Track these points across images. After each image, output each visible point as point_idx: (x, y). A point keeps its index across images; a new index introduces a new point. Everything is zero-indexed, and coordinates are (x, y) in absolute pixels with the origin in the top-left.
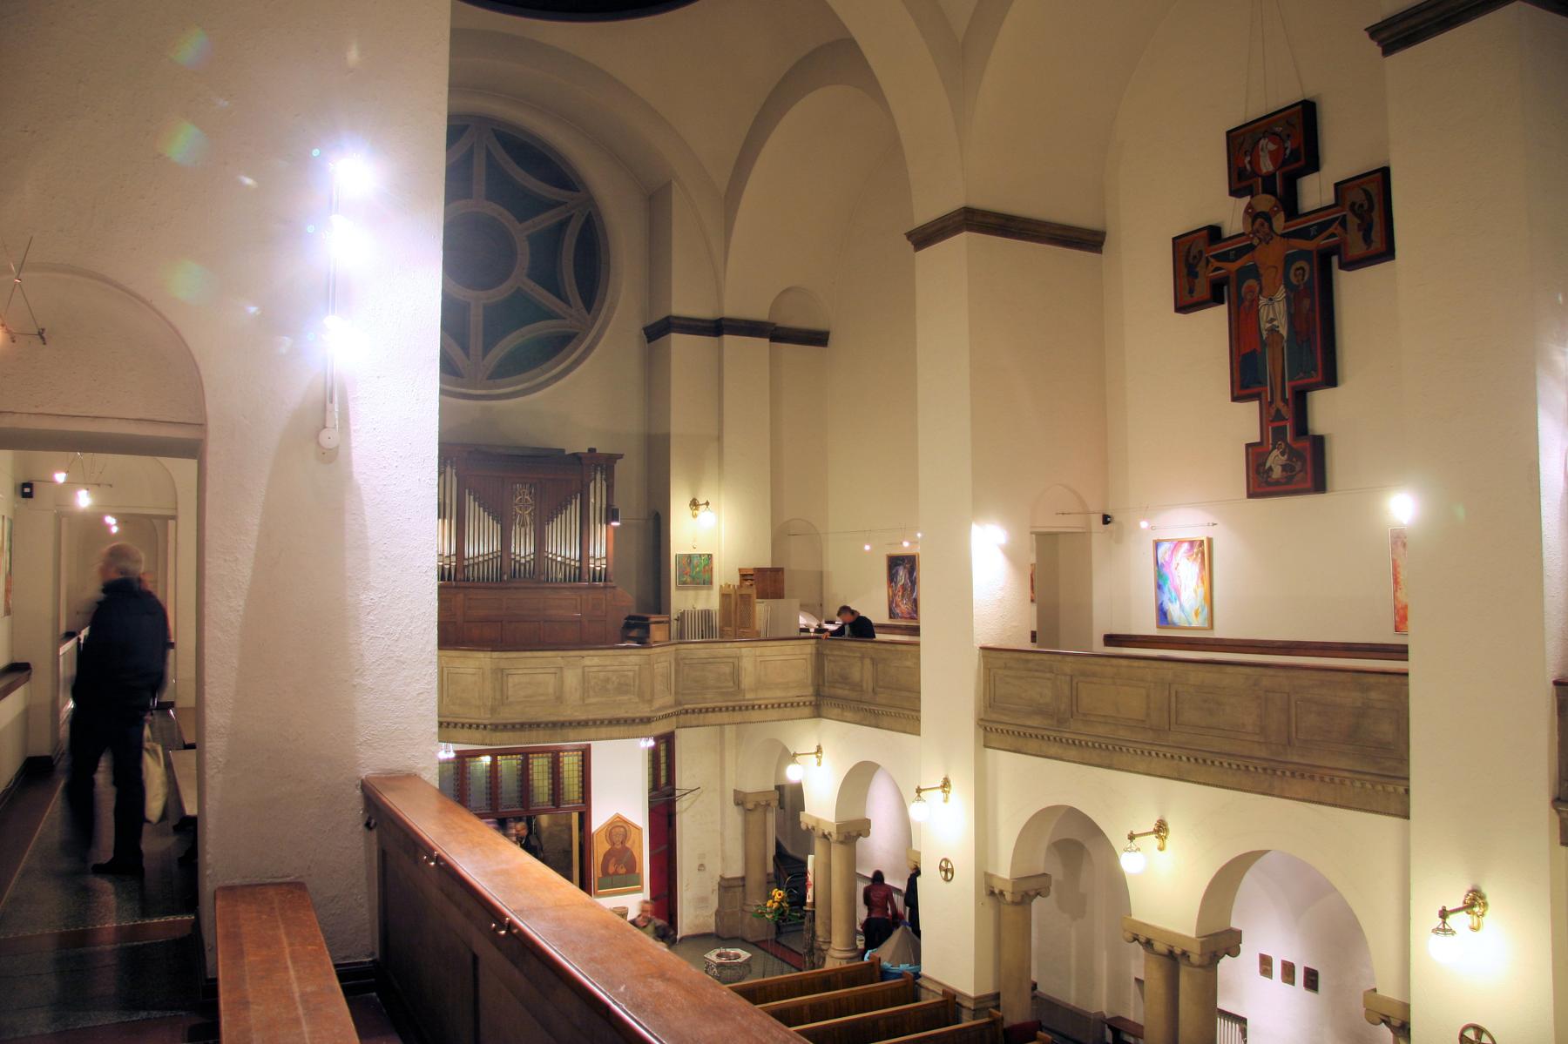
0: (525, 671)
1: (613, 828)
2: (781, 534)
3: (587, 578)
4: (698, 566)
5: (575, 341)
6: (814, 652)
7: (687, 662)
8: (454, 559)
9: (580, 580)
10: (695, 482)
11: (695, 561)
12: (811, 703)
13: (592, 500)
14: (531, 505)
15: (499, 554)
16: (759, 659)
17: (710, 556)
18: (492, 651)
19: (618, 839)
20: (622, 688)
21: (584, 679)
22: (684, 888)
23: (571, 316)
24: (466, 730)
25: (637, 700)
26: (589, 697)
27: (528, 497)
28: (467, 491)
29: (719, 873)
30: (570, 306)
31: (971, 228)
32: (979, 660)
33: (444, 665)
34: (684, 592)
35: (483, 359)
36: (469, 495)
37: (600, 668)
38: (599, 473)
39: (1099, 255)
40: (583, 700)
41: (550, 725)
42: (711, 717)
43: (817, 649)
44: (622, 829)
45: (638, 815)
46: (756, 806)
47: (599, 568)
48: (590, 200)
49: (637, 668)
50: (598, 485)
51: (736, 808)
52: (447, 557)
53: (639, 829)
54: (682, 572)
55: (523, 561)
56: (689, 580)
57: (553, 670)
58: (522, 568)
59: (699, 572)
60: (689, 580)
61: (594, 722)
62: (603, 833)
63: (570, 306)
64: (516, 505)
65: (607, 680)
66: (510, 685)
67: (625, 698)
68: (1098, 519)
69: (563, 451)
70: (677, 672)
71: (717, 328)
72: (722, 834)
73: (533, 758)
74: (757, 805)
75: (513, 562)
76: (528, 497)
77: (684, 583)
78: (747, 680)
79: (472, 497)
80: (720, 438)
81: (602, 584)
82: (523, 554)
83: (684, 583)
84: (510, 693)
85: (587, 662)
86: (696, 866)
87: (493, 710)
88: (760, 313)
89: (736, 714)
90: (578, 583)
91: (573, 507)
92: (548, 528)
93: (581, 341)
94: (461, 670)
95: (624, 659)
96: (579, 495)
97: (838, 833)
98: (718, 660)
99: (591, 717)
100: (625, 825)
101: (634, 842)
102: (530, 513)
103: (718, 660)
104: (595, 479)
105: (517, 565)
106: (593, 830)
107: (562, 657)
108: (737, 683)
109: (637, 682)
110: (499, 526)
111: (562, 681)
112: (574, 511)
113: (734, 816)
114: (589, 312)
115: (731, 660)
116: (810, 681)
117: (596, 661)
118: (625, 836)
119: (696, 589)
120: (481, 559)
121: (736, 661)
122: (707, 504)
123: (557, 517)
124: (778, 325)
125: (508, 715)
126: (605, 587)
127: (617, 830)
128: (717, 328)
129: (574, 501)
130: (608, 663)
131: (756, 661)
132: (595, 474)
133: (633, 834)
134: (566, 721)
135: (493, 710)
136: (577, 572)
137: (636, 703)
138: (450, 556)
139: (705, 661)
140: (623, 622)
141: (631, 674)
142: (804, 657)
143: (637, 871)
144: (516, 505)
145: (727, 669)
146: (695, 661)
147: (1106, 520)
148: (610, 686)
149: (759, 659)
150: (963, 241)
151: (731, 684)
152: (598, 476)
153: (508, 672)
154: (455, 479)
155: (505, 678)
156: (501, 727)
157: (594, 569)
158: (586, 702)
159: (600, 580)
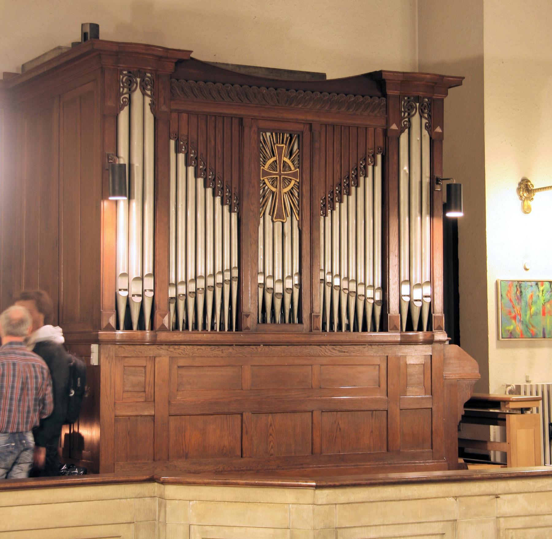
8: (149, 283)
9: (384, 328)
13: (404, 168)
14: (294, 175)
15: (235, 273)
18: (317, 487)
27: (286, 160)
33: (194, 521)
34: (509, 352)
36: (177, 151)
38: (417, 116)
47: (419, 304)
50: (415, 138)
52: (136, 279)
55: (279, 289)
58: (278, 302)
59: (536, 314)
64: (266, 174)
69: (324, 75)
75: (261, 291)
76: (286, 160)
77: (511, 335)
81: (421, 335)
82: (278, 276)
83: (511, 335)
90: (377, 334)
91: (369, 180)
96: (379, 157)
102: (291, 192)
105: (269, 297)
110: (234, 216)
119: (530, 346)
120: (201, 284)
123: (341, 201)
129: (370, 168)
138: (142, 279)
140: (461, 411)
144: (266, 174)
159: (420, 328)
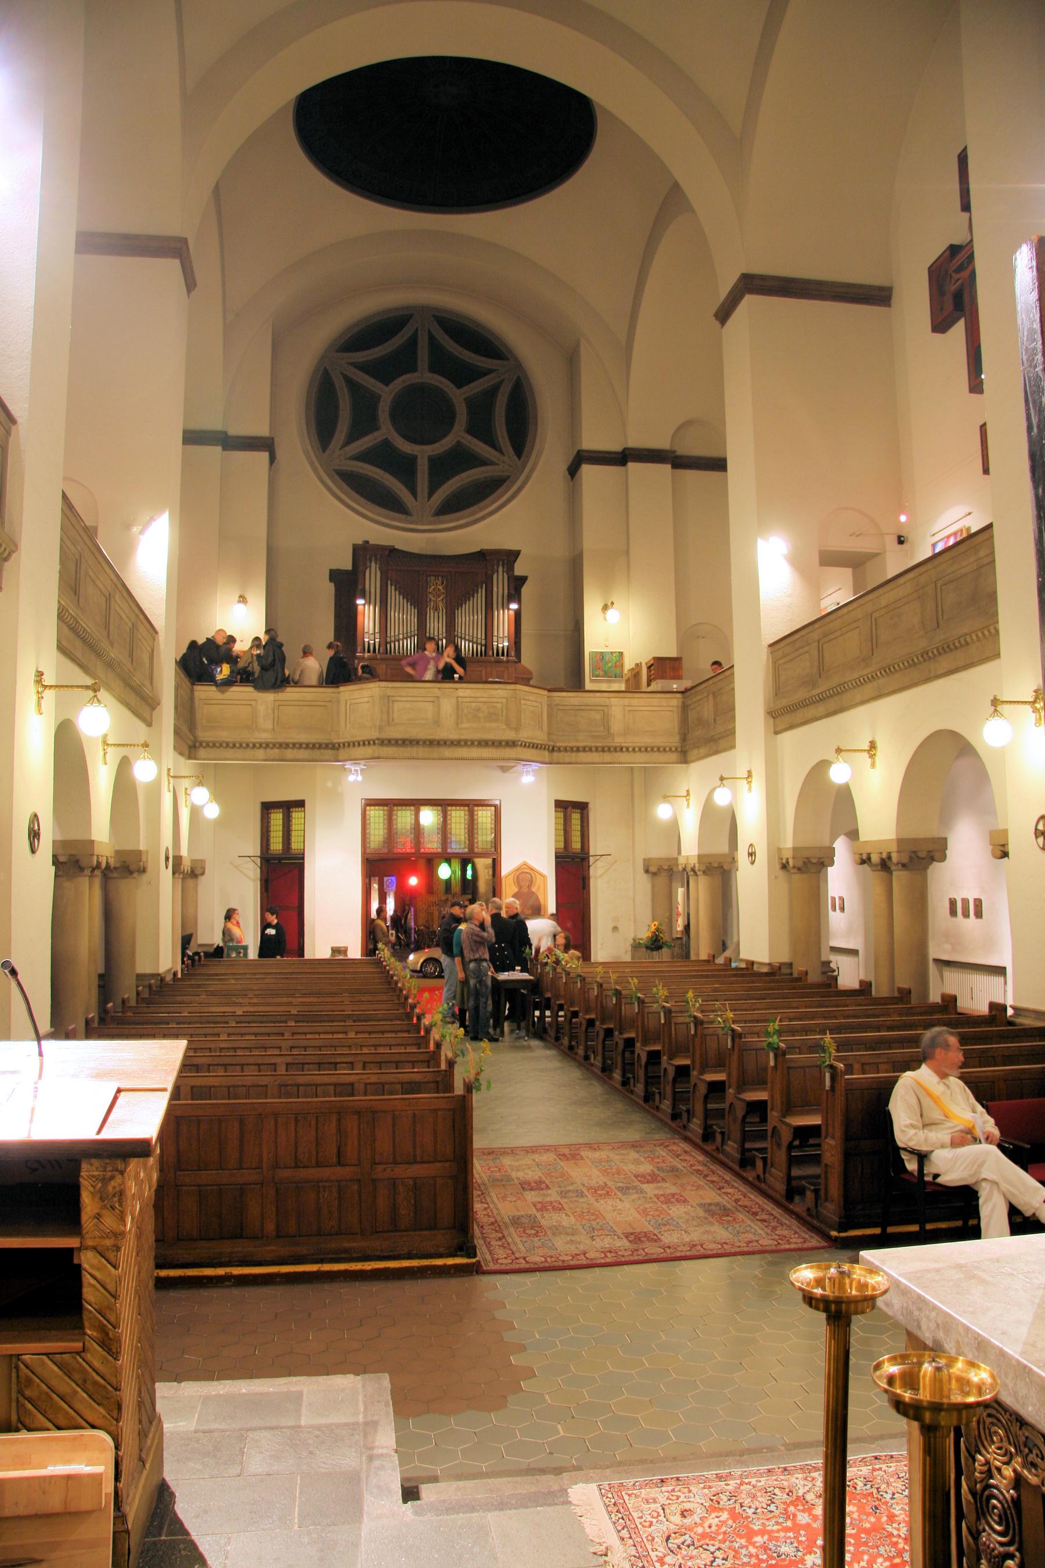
2: (686, 635)
3: (491, 653)
4: (609, 662)
5: (508, 482)
6: (680, 705)
7: (561, 708)
8: (377, 636)
10: (606, 585)
11: (607, 658)
12: (676, 749)
13: (495, 589)
16: (628, 708)
17: (621, 654)
20: (492, 717)
21: (458, 707)
22: (599, 947)
23: (504, 462)
24: (362, 747)
25: (505, 727)
26: (462, 722)
28: (389, 582)
29: (632, 936)
30: (503, 454)
31: (752, 291)
32: (768, 657)
35: (429, 500)
36: (391, 585)
37: (472, 699)
39: (887, 309)
40: (457, 725)
42: (583, 756)
43: (683, 703)
44: (528, 876)
45: (546, 867)
46: (659, 869)
48: (519, 366)
49: (504, 700)
50: (500, 577)
51: (645, 875)
53: (544, 876)
54: (595, 667)
56: (601, 673)
57: (431, 699)
60: (601, 673)
61: (466, 742)
63: (503, 454)
65: (478, 710)
66: (396, 710)
67: (494, 725)
68: (891, 542)
70: (550, 716)
71: (622, 458)
72: (634, 900)
73: (450, 811)
74: (660, 869)
78: (616, 726)
80: (628, 552)
81: (505, 658)
84: (395, 716)
85: (461, 693)
86: (610, 927)
87: (381, 728)
88: (661, 442)
89: (606, 754)
92: (458, 613)
93: (514, 483)
94: (359, 701)
97: (699, 863)
98: (589, 708)
99: (462, 737)
101: (539, 887)
103: (589, 708)
104: (498, 571)
106: (502, 875)
107: (439, 688)
108: (607, 728)
109: (505, 712)
111: (439, 707)
112: (480, 596)
113: (644, 883)
114: (519, 457)
115: (601, 708)
116: (677, 729)
117: (468, 693)
118: (531, 882)
121: (606, 709)
122: (612, 603)
124: (677, 453)
125: (394, 733)
126: (508, 662)
127: (524, 875)
128: (622, 458)
130: (478, 695)
131: (624, 710)
132: (498, 568)
133: (539, 881)
135: (381, 728)
136: (483, 648)
139: (577, 708)
141: (499, 705)
142: (671, 709)
145: (598, 717)
147: (901, 541)
148: (481, 715)
149: (628, 708)
150: (749, 302)
151: (602, 729)
152: (500, 569)
153: (393, 698)
154: (379, 573)
155: (391, 704)
156: (386, 742)
157: (503, 647)
159: (503, 655)
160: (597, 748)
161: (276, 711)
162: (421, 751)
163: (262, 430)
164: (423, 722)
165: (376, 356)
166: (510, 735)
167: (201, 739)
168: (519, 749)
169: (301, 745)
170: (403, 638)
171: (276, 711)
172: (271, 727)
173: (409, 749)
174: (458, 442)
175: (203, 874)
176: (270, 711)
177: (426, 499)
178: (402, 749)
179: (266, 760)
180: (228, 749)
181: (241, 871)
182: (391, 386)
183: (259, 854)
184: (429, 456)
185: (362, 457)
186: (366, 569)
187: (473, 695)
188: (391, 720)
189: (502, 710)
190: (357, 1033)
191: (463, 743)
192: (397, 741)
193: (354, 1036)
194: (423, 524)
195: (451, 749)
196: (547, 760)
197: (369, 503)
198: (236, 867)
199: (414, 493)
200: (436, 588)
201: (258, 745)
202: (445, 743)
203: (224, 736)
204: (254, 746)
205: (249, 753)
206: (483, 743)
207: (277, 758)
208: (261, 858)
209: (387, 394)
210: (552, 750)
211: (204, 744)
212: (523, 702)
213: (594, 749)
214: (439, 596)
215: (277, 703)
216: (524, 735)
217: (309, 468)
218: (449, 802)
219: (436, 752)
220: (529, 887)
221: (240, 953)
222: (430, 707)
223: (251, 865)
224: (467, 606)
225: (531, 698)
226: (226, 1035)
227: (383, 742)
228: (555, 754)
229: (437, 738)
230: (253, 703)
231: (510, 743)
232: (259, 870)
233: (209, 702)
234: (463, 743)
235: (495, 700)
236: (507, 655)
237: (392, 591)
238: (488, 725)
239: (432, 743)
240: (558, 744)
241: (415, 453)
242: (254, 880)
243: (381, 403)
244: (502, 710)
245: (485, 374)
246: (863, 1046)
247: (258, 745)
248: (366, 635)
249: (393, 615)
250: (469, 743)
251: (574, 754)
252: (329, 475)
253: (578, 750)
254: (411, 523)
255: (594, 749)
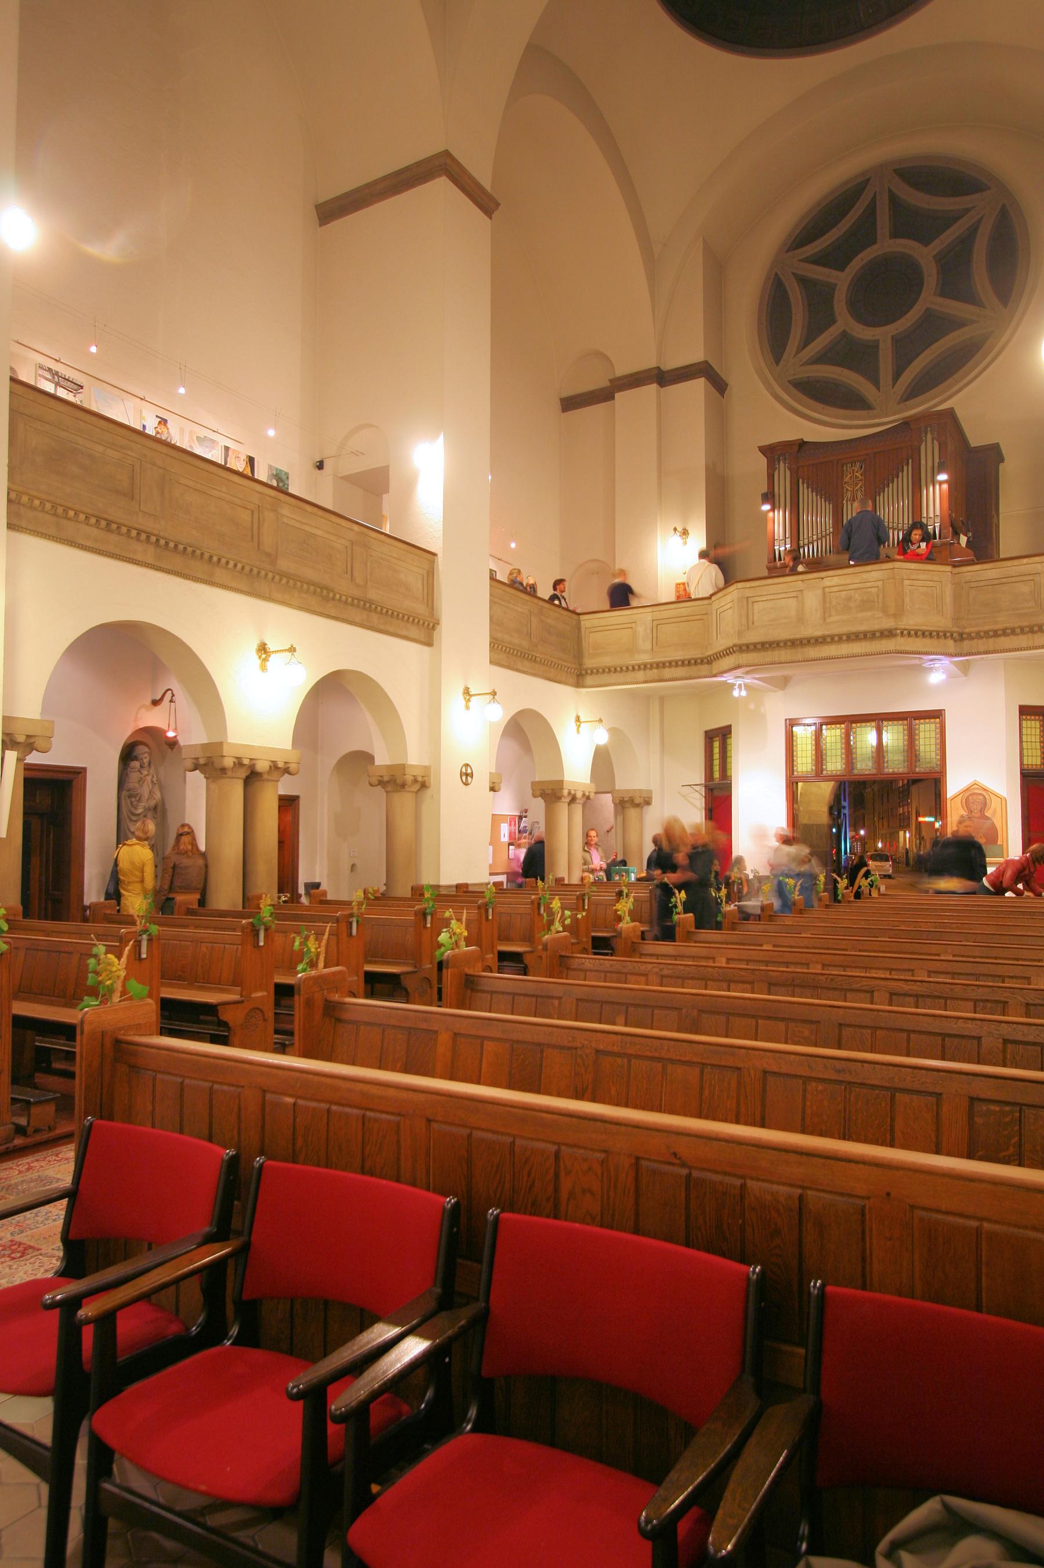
0: (769, 597)
1: (970, 795)
7: (972, 585)
8: (788, 541)
13: (923, 462)
14: (861, 480)
19: (976, 808)
25: (881, 615)
28: (801, 480)
36: (803, 483)
37: (840, 588)
41: (789, 644)
44: (981, 797)
49: (880, 584)
53: (1003, 801)
57: (794, 594)
61: (832, 637)
62: (959, 798)
65: (849, 599)
66: (756, 611)
67: (868, 614)
79: (805, 485)
84: (756, 618)
85: (827, 582)
95: (865, 576)
98: (1014, 579)
99: (827, 633)
100: (984, 793)
101: (995, 812)
103: (1014, 579)
107: (802, 581)
109: (881, 597)
110: (831, 505)
112: (906, 476)
115: (1030, 578)
117: (836, 581)
118: (985, 805)
125: (753, 637)
130: (848, 581)
132: (926, 434)
133: (994, 804)
134: (797, 640)
135: (740, 634)
137: (880, 617)
139: (996, 582)
143: (999, 843)
146: (983, 583)
152: (929, 436)
154: (788, 473)
158: (828, 621)
160: (1022, 629)
161: (655, 630)
162: (783, 654)
163: (694, 353)
164: (786, 621)
165: (826, 244)
166: (888, 623)
167: (589, 666)
168: (900, 640)
169: (677, 662)
170: (818, 539)
171: (655, 630)
172: (650, 647)
173: (770, 653)
174: (928, 309)
175: (499, 791)
176: (649, 631)
177: (891, 386)
178: (762, 654)
179: (646, 682)
180: (612, 674)
181: (689, 801)
182: (847, 270)
183: (703, 782)
184: (893, 337)
185: (821, 359)
186: (774, 471)
187: (842, 582)
188: (750, 623)
189: (878, 596)
190: (728, 960)
191: (829, 640)
192: (755, 645)
193: (724, 965)
194: (887, 416)
195: (817, 648)
196: (952, 650)
197: (826, 407)
198: (684, 796)
199: (876, 384)
200: (853, 476)
201: (636, 667)
202: (809, 641)
203: (607, 661)
204: (634, 669)
205: (630, 676)
206: (853, 637)
207: (656, 678)
208: (706, 786)
209: (842, 280)
210: (962, 637)
211: (589, 671)
212: (906, 582)
213: (1018, 631)
214: (857, 484)
215: (655, 623)
216: (910, 622)
217: (761, 385)
218: (884, 716)
219: (800, 653)
220: (982, 811)
221: (623, 876)
222: (792, 603)
223: (697, 796)
224: (889, 491)
225: (921, 577)
226: (819, 966)
227: (741, 648)
228: (966, 643)
229: (798, 636)
230: (633, 625)
231: (886, 633)
232: (704, 799)
233: (594, 629)
234: (829, 640)
235: (868, 585)
236: (940, 538)
237: (804, 491)
238: (860, 615)
239: (794, 643)
240: (967, 630)
241: (877, 338)
242: (701, 810)
243: (837, 293)
244: (878, 596)
245: (959, 218)
246: (643, 978)
247: (636, 667)
248: (776, 543)
249: (805, 518)
250: (836, 639)
251: (991, 640)
252: (782, 386)
253: (996, 634)
254: (875, 417)
255: (1018, 631)
